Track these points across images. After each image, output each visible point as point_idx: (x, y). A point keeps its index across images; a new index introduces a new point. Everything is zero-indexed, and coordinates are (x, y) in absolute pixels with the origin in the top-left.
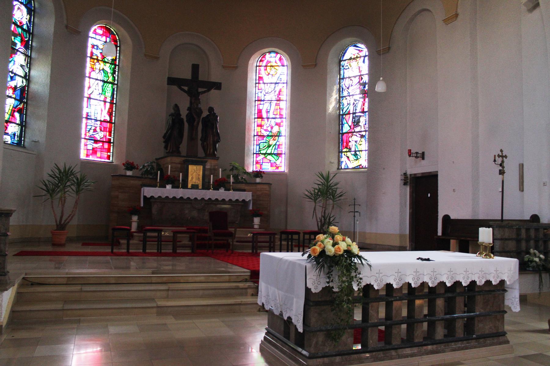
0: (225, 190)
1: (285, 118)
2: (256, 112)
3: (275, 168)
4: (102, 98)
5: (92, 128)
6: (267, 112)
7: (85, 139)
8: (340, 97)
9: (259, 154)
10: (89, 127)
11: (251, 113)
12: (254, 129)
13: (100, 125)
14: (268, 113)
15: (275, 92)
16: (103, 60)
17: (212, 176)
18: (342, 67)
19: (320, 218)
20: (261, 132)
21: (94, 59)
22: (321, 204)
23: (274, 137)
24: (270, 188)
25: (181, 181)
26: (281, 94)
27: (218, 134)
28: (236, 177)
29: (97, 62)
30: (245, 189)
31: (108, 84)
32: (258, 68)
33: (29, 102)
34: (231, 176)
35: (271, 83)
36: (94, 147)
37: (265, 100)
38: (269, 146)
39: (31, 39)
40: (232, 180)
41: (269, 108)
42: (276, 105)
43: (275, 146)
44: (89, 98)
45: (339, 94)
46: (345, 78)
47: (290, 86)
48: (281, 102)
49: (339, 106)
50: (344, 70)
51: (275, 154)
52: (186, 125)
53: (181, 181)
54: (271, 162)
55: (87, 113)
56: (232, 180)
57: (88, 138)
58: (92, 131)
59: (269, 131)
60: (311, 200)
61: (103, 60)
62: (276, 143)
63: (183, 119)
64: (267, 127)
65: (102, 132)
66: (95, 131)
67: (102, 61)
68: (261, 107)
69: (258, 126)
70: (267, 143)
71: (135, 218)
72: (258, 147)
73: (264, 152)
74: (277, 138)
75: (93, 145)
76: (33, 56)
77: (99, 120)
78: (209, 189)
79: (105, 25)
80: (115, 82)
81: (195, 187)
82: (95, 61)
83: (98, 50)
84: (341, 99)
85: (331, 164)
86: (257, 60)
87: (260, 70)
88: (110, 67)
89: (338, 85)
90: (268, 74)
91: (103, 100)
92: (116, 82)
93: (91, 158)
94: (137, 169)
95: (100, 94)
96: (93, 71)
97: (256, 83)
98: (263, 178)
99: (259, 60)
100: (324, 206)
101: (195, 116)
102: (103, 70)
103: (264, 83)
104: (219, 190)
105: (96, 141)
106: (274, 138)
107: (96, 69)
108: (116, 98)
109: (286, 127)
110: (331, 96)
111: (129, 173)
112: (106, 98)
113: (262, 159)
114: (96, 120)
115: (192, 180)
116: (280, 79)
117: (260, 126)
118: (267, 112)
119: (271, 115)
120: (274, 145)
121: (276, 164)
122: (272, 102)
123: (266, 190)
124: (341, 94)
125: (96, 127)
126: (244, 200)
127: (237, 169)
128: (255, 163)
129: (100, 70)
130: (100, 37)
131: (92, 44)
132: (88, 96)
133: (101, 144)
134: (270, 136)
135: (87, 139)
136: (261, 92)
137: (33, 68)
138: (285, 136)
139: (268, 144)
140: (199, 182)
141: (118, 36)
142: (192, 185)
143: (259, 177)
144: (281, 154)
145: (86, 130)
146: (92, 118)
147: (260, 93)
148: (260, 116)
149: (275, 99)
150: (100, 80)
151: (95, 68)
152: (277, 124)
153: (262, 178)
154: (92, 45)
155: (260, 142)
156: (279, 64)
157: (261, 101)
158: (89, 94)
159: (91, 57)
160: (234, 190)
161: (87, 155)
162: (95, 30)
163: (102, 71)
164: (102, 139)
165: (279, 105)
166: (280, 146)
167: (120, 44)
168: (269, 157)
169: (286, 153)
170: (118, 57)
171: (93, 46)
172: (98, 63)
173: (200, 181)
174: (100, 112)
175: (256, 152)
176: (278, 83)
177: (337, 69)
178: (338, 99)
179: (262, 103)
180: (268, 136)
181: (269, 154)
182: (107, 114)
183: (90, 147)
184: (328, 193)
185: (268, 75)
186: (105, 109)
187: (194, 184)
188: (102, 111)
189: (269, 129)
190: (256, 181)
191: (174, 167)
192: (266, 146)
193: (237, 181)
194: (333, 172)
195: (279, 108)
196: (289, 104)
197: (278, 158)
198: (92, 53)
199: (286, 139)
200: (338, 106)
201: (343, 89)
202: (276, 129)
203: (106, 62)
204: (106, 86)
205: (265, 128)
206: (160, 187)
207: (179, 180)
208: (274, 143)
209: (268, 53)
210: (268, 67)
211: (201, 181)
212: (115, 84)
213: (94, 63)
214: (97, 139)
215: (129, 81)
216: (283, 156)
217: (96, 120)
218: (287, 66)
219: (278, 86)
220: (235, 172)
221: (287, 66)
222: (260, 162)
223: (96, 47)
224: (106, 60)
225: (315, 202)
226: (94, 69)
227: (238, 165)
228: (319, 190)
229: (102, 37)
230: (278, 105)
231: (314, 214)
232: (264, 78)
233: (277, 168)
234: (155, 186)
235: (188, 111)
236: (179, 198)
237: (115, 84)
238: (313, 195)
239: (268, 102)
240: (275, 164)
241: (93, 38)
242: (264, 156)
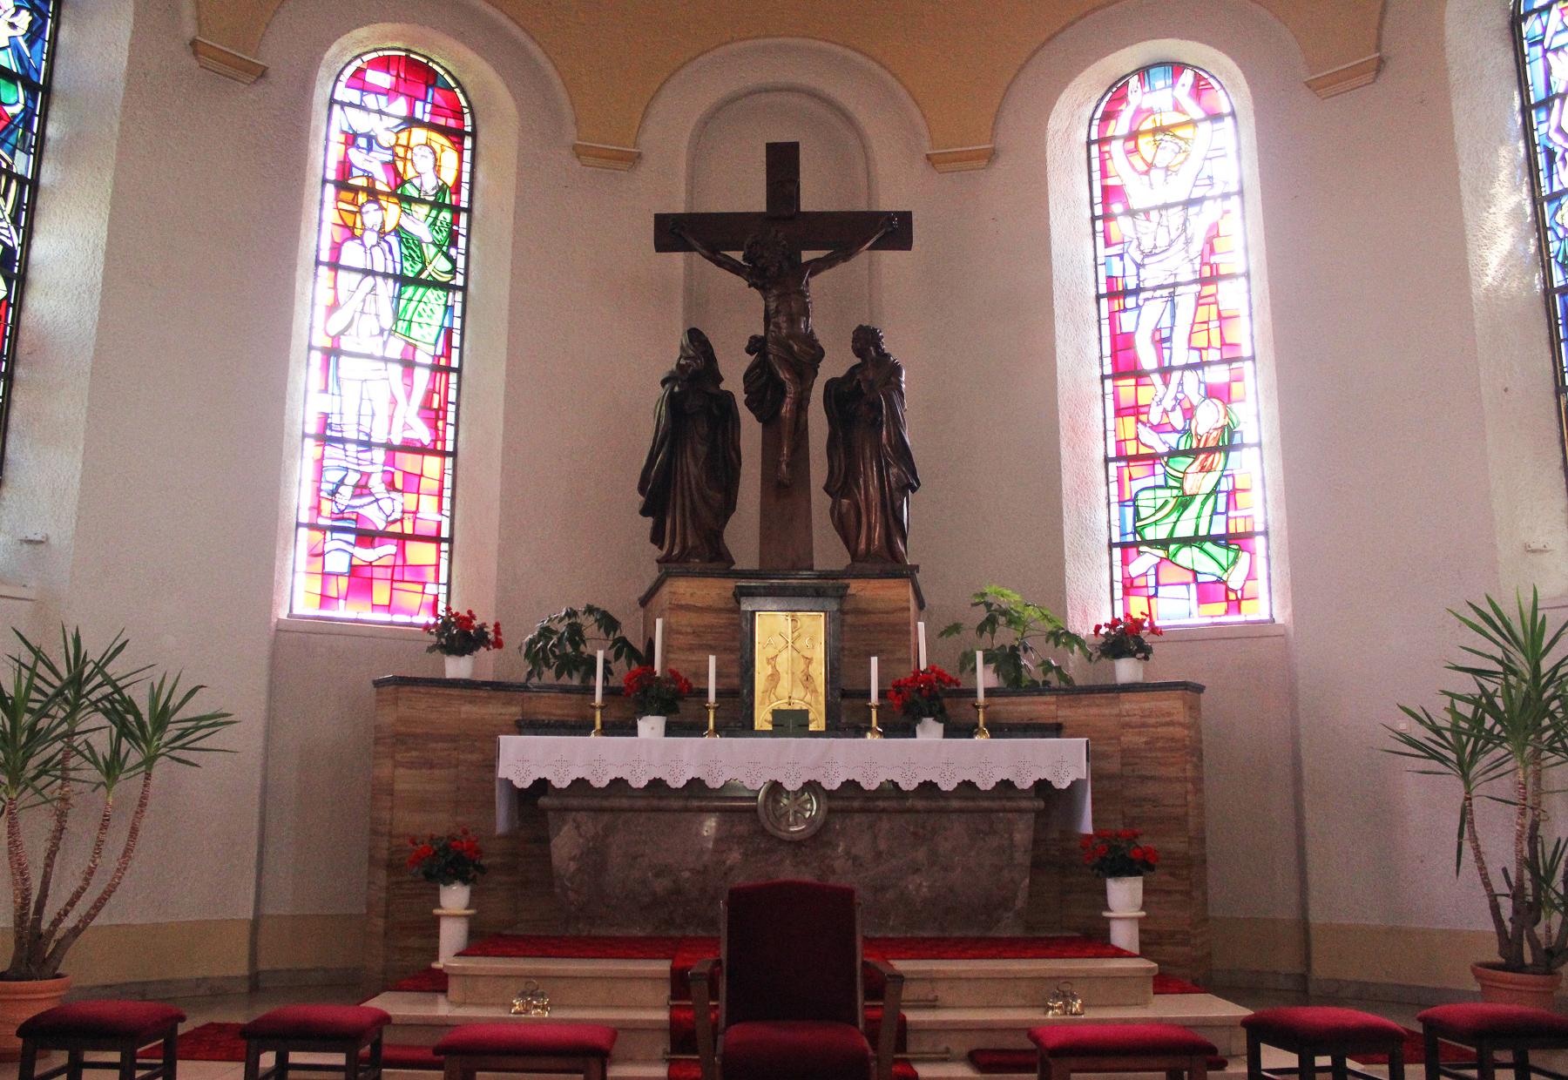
0: (948, 733)
1: (1253, 358)
2: (1107, 350)
3: (1224, 605)
4: (396, 348)
5: (346, 482)
6: (1160, 342)
7: (313, 527)
8: (1537, 201)
9: (1135, 544)
10: (332, 476)
11: (1080, 351)
12: (1102, 429)
13: (385, 464)
14: (1164, 345)
15: (1188, 242)
16: (399, 192)
17: (874, 660)
18: (1531, 45)
19: (1505, 871)
20: (1137, 438)
21: (356, 190)
22: (1505, 786)
23: (1202, 457)
24: (1194, 708)
25: (874, 698)
26: (1217, 249)
27: (903, 454)
28: (1007, 661)
29: (369, 201)
30: (1059, 720)
31: (421, 290)
32: (1095, 149)
33: (20, 372)
34: (979, 655)
35: (1166, 206)
36: (356, 562)
37: (1144, 290)
38: (1184, 503)
39: (38, 113)
40: (984, 678)
41: (1166, 322)
42: (1198, 305)
43: (1212, 499)
44: (332, 353)
45: (1534, 185)
46: (1558, 95)
47: (1259, 196)
48: (1223, 286)
49: (1540, 248)
50: (1544, 57)
51: (1215, 540)
52: (750, 431)
53: (874, 698)
54: (1201, 578)
55: (326, 416)
56: (984, 678)
57: (329, 523)
58: (346, 492)
59: (1175, 430)
60: (1434, 765)
61: (399, 192)
62: (1218, 483)
63: (729, 396)
64: (1165, 412)
65: (394, 495)
66: (362, 489)
67: (393, 194)
68: (1127, 323)
69: (1120, 412)
70: (1171, 488)
71: (455, 898)
72: (1129, 512)
73: (1162, 533)
74: (1219, 458)
75: (352, 555)
76: (46, 178)
77: (380, 445)
78: (858, 730)
79: (403, 54)
80: (454, 278)
81: (790, 723)
82: (362, 198)
83: (372, 154)
84: (1548, 209)
85: (1530, 556)
86: (1088, 114)
87: (1107, 156)
88: (430, 220)
89: (1521, 144)
90: (1145, 168)
91: (399, 357)
92: (460, 281)
93: (347, 611)
94: (498, 644)
95: (382, 331)
96: (353, 237)
97: (1094, 219)
98: (1151, 656)
99: (1098, 115)
100: (1529, 802)
101: (783, 375)
102: (398, 230)
103: (1130, 213)
104: (915, 736)
105: (367, 537)
106: (1206, 459)
107: (364, 229)
108: (461, 348)
109: (1261, 397)
110: (1489, 202)
111: (457, 667)
112: (415, 348)
113: (1152, 571)
114: (368, 445)
115: (775, 687)
116: (1208, 182)
117: (1132, 411)
118: (1160, 342)
119: (1180, 354)
120: (1208, 495)
121: (1228, 589)
122: (1179, 290)
123: (1171, 724)
124: (1544, 181)
125: (369, 475)
126: (1042, 786)
127: (1013, 620)
128: (1118, 593)
129: (382, 234)
130: (383, 99)
131: (346, 128)
132: (328, 343)
133: (390, 548)
134: (1185, 453)
135: (323, 529)
136: (1121, 256)
137: (41, 226)
138: (1259, 445)
139: (1175, 492)
140: (808, 698)
141: (464, 92)
142: (776, 713)
143: (1132, 654)
144: (1249, 535)
145: (319, 490)
146: (346, 435)
147: (1116, 261)
148: (1124, 365)
149: (1192, 277)
150: (385, 275)
151: (359, 225)
152: (1212, 392)
153: (1146, 658)
154: (343, 132)
155: (1136, 486)
156: (1195, 112)
157: (1126, 293)
158: (332, 334)
159: (342, 184)
160: (999, 729)
161: (325, 600)
162: (359, 73)
163: (393, 240)
164: (399, 524)
165: (1216, 303)
166: (1239, 496)
167: (474, 125)
168: (1187, 556)
169: (1271, 530)
170: (466, 177)
171: (351, 139)
172: (373, 206)
173: (815, 691)
174: (383, 411)
175: (1123, 534)
176: (1199, 201)
177: (1507, 59)
178: (1528, 209)
179: (1130, 302)
180: (1174, 453)
181: (1186, 542)
182: (418, 414)
183: (338, 563)
184: (1546, 722)
185: (1147, 173)
186: (409, 395)
187: (785, 707)
188: (394, 402)
189: (1177, 420)
190: (1113, 671)
191: (689, 630)
192: (1166, 502)
193: (1014, 680)
194: (1555, 598)
195: (1214, 316)
196: (1260, 284)
197: (1232, 554)
198: (346, 168)
199: (1265, 456)
200: (1532, 249)
201: (1550, 155)
202: (1208, 418)
203: (410, 200)
204: (410, 300)
205: (1155, 417)
206: (609, 729)
207: (705, 692)
208: (1208, 482)
209: (1136, 77)
210: (1142, 141)
211: (822, 689)
212: (455, 288)
213: (356, 205)
214: (372, 528)
215: (508, 266)
216: (1259, 543)
217: (368, 445)
218: (1233, 114)
219: (1197, 214)
220: (1005, 636)
221: (1233, 114)
222: (1147, 586)
223: (362, 142)
224: (410, 190)
225: (1465, 776)
226: (358, 232)
227: (1017, 597)
228: (1484, 703)
229: (390, 101)
230: (1209, 304)
231: (1467, 846)
232: (1128, 190)
233: (1235, 606)
234: (581, 727)
235: (751, 354)
236: (681, 783)
237: (455, 288)
238: (1448, 735)
239: (1158, 293)
240: (1224, 587)
241: (351, 105)
242: (1162, 553)
